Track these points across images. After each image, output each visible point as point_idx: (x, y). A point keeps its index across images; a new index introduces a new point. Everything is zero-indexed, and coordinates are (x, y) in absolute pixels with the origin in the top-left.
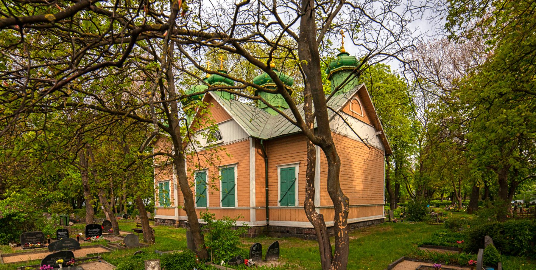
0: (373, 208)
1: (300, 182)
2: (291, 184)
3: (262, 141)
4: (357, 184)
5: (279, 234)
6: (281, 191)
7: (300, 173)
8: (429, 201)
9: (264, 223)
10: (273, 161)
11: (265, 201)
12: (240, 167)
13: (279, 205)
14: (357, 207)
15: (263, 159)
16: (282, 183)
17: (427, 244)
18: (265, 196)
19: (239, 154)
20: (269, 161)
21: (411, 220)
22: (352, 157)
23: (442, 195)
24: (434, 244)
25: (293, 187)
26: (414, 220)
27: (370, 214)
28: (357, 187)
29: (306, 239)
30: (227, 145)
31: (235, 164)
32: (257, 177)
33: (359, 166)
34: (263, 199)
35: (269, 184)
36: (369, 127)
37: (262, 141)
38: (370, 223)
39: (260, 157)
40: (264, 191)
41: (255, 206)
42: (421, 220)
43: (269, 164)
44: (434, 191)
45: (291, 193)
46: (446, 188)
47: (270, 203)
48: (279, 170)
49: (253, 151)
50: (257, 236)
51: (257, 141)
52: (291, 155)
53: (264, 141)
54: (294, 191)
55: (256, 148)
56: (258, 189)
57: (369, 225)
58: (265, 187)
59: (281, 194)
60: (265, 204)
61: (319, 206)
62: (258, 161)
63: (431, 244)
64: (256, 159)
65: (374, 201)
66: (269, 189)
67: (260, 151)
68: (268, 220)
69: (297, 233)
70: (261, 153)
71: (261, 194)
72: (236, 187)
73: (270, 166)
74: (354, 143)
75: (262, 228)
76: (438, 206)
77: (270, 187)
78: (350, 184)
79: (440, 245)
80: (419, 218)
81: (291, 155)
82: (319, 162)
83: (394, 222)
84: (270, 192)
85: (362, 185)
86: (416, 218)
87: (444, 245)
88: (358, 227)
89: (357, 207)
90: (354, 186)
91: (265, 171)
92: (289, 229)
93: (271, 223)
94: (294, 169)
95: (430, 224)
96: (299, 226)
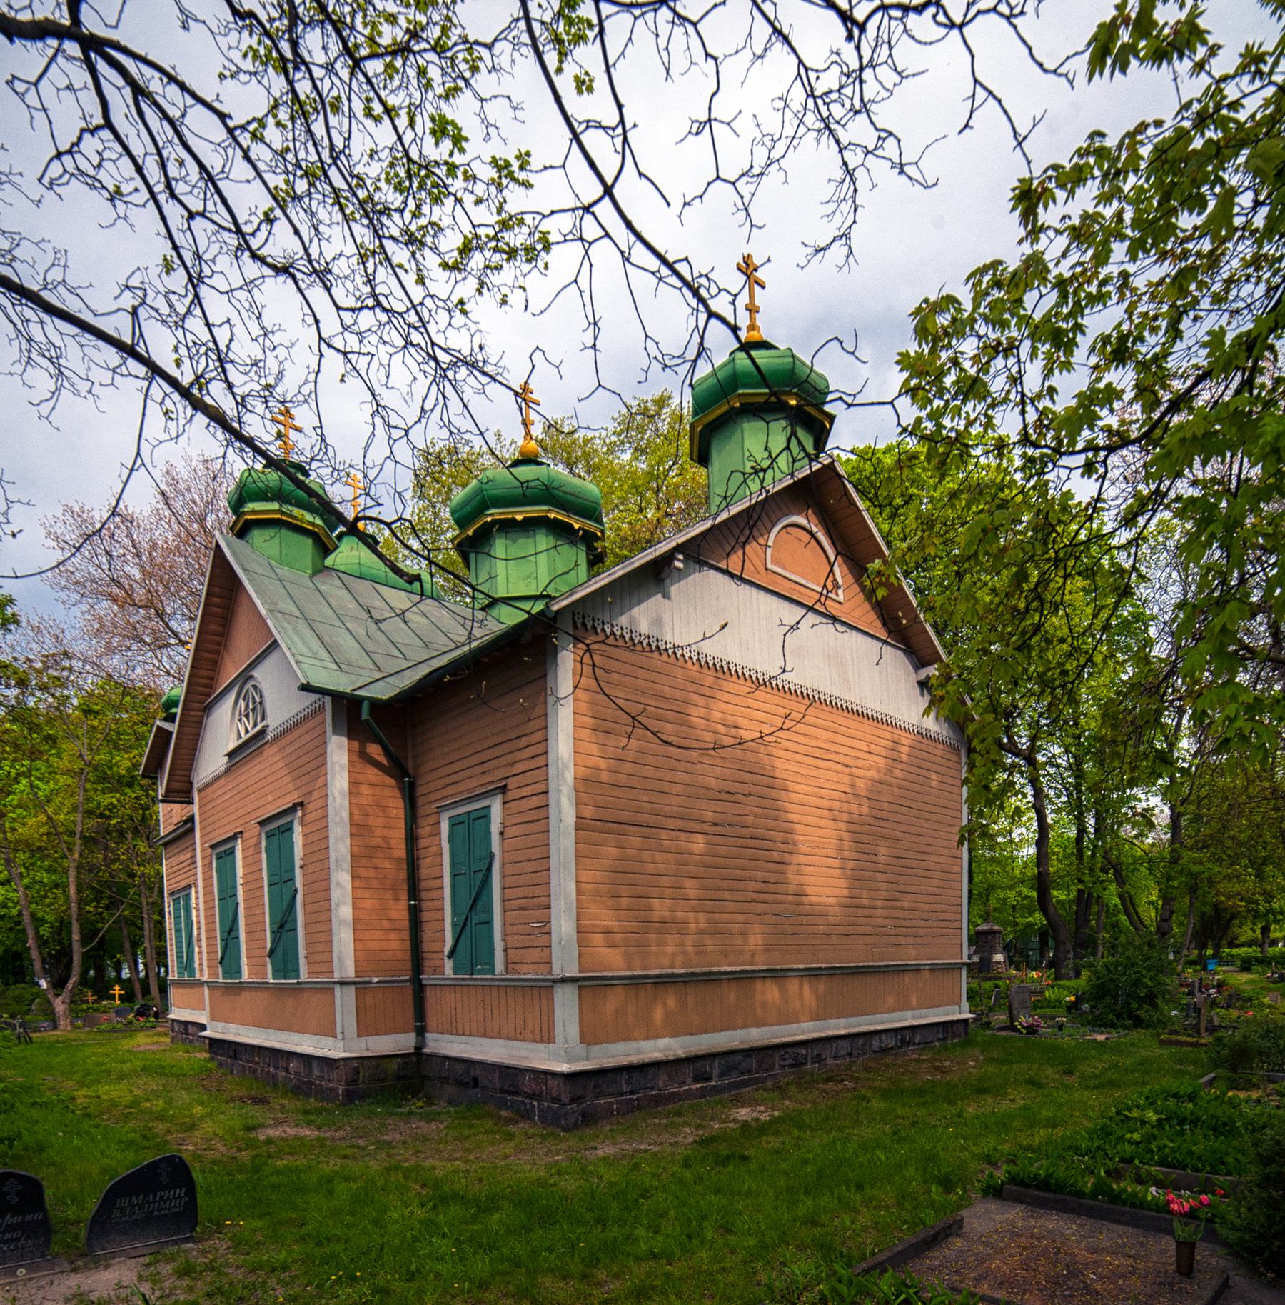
0: (907, 979)
1: (510, 869)
2: (480, 875)
3: (365, 706)
4: (806, 880)
5: (450, 1090)
6: (454, 914)
7: (510, 832)
8: (1217, 948)
9: (402, 1042)
10: (432, 786)
11: (407, 956)
12: (309, 818)
13: (449, 966)
14: (812, 974)
15: (390, 781)
16: (454, 876)
17: (1022, 1183)
18: (406, 935)
19: (302, 771)
20: (420, 790)
21: (1100, 1023)
22: (777, 763)
23: (1265, 930)
24: (1060, 1188)
25: (484, 898)
26: (1113, 1026)
27: (890, 1001)
28: (809, 890)
29: (526, 1116)
30: (281, 735)
31: (293, 809)
32: (361, 857)
33: (825, 803)
34: (397, 945)
35: (423, 885)
36: (887, 649)
37: (365, 706)
38: (890, 1042)
39: (373, 774)
40: (400, 911)
41: (350, 973)
42: (1138, 1023)
43: (420, 801)
44: (1233, 917)
45: (482, 917)
46: (1276, 906)
47: (427, 963)
48: (445, 827)
49: (339, 751)
50: (362, 1097)
51: (349, 712)
52: (476, 759)
53: (375, 704)
54: (489, 911)
55: (349, 738)
56: (368, 904)
57: (884, 1051)
58: (404, 895)
59: (454, 924)
60: (409, 966)
61: (573, 971)
62: (365, 790)
63: (1044, 1184)
64: (354, 783)
65: (912, 951)
66: (425, 905)
67: (374, 750)
68: (421, 1032)
69: (503, 1091)
70: (382, 759)
71: (386, 924)
72: (299, 897)
73: (421, 811)
74: (851, 723)
75: (394, 1065)
76: (1246, 966)
77: (424, 895)
78: (772, 877)
79: (1094, 1195)
80: (1131, 1016)
81: (476, 759)
82: (569, 776)
83: (1032, 1030)
84: (425, 916)
85: (843, 883)
86: (1119, 1016)
87: (1116, 1198)
88: (819, 1059)
89: (812, 974)
90: (791, 889)
91: (401, 834)
92: (476, 1072)
93: (445, 1044)
94: (485, 815)
95: (1170, 1043)
96: (506, 1062)
